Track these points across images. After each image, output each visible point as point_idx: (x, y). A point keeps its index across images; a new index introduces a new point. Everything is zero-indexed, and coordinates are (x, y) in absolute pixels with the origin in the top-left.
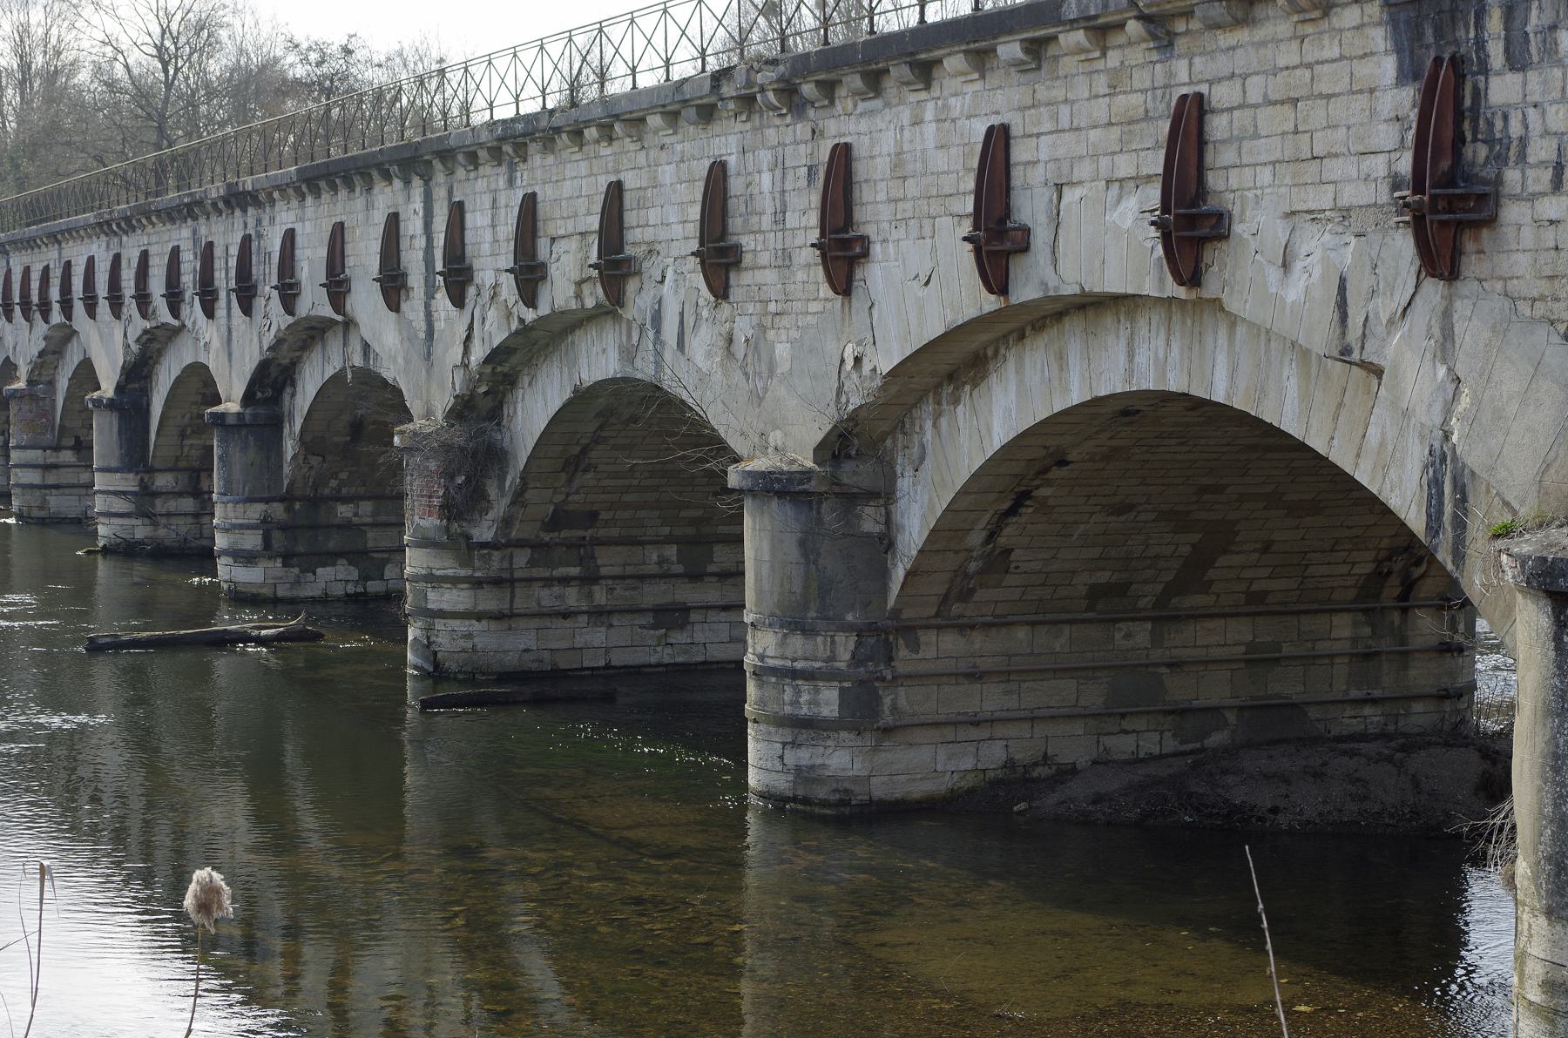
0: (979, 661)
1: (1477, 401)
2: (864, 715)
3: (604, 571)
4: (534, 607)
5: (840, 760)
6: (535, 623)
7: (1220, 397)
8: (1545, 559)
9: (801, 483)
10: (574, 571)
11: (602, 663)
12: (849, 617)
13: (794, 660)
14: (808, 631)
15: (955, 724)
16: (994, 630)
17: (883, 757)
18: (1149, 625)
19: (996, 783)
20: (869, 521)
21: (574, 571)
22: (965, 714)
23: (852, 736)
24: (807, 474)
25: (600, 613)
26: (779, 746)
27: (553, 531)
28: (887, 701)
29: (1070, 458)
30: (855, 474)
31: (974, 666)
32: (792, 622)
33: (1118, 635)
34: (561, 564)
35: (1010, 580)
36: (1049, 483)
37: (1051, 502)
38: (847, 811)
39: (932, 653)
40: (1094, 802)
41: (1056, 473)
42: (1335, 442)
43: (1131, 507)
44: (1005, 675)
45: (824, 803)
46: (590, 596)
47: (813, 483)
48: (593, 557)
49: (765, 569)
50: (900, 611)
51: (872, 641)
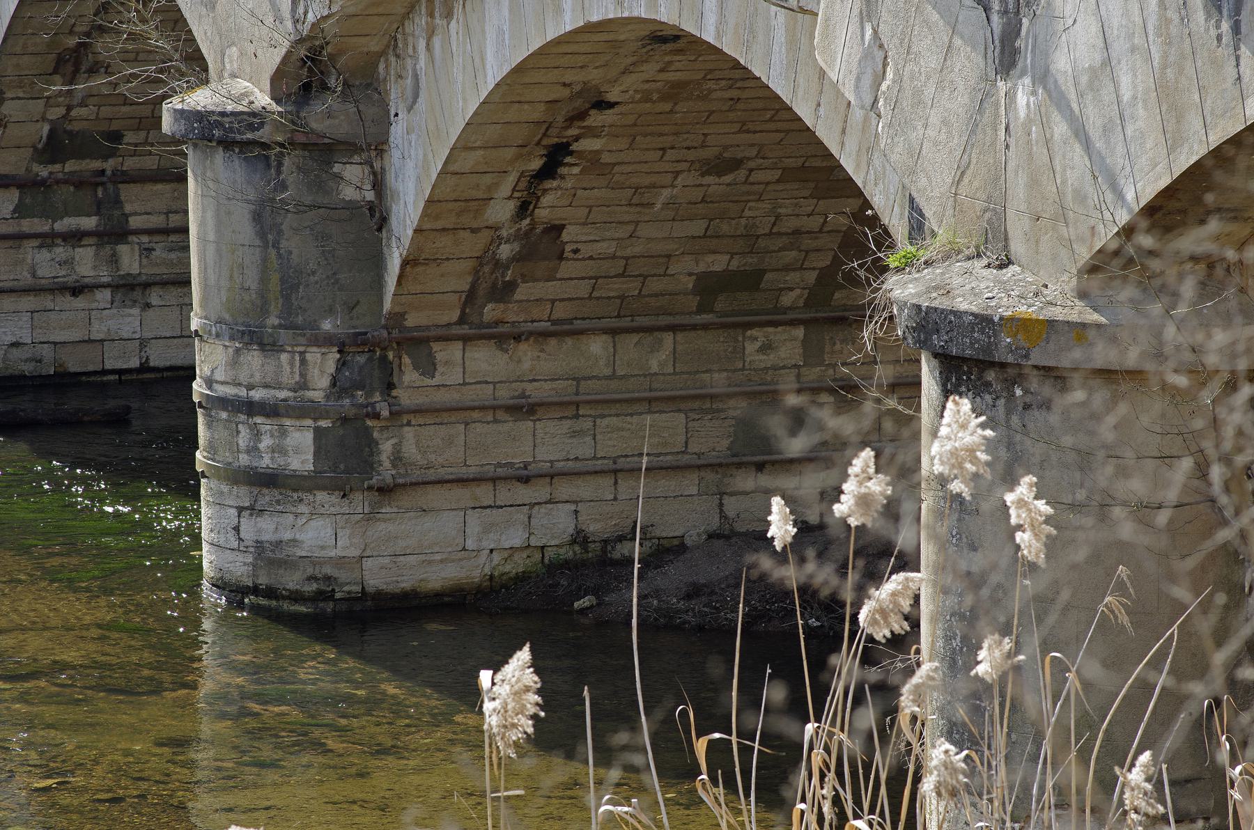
0: (530, 388)
1: (898, 79)
2: (350, 464)
3: (135, 222)
4: (25, 278)
5: (321, 535)
6: (28, 302)
7: (709, 37)
8: (919, 307)
9: (252, 128)
10: (89, 223)
11: (134, 363)
12: (327, 326)
13: (250, 387)
14: (269, 346)
15: (494, 480)
16: (553, 342)
17: (381, 529)
18: (800, 332)
19: (555, 568)
20: (352, 180)
21: (89, 223)
22: (511, 465)
23: (335, 498)
24: (255, 118)
25: (131, 287)
26: (234, 512)
27: (53, 162)
28: (386, 447)
29: (612, 97)
30: (329, 115)
31: (523, 395)
32: (250, 334)
33: (751, 348)
34: (67, 214)
35: (566, 269)
36: (593, 133)
37: (606, 158)
38: (329, 607)
39: (455, 377)
40: (688, 597)
41: (597, 119)
42: (822, 109)
43: (736, 164)
44: (570, 407)
45: (296, 597)
46: (114, 260)
47: (267, 128)
48: (118, 202)
49: (211, 249)
50: (402, 315)
51: (361, 359)
